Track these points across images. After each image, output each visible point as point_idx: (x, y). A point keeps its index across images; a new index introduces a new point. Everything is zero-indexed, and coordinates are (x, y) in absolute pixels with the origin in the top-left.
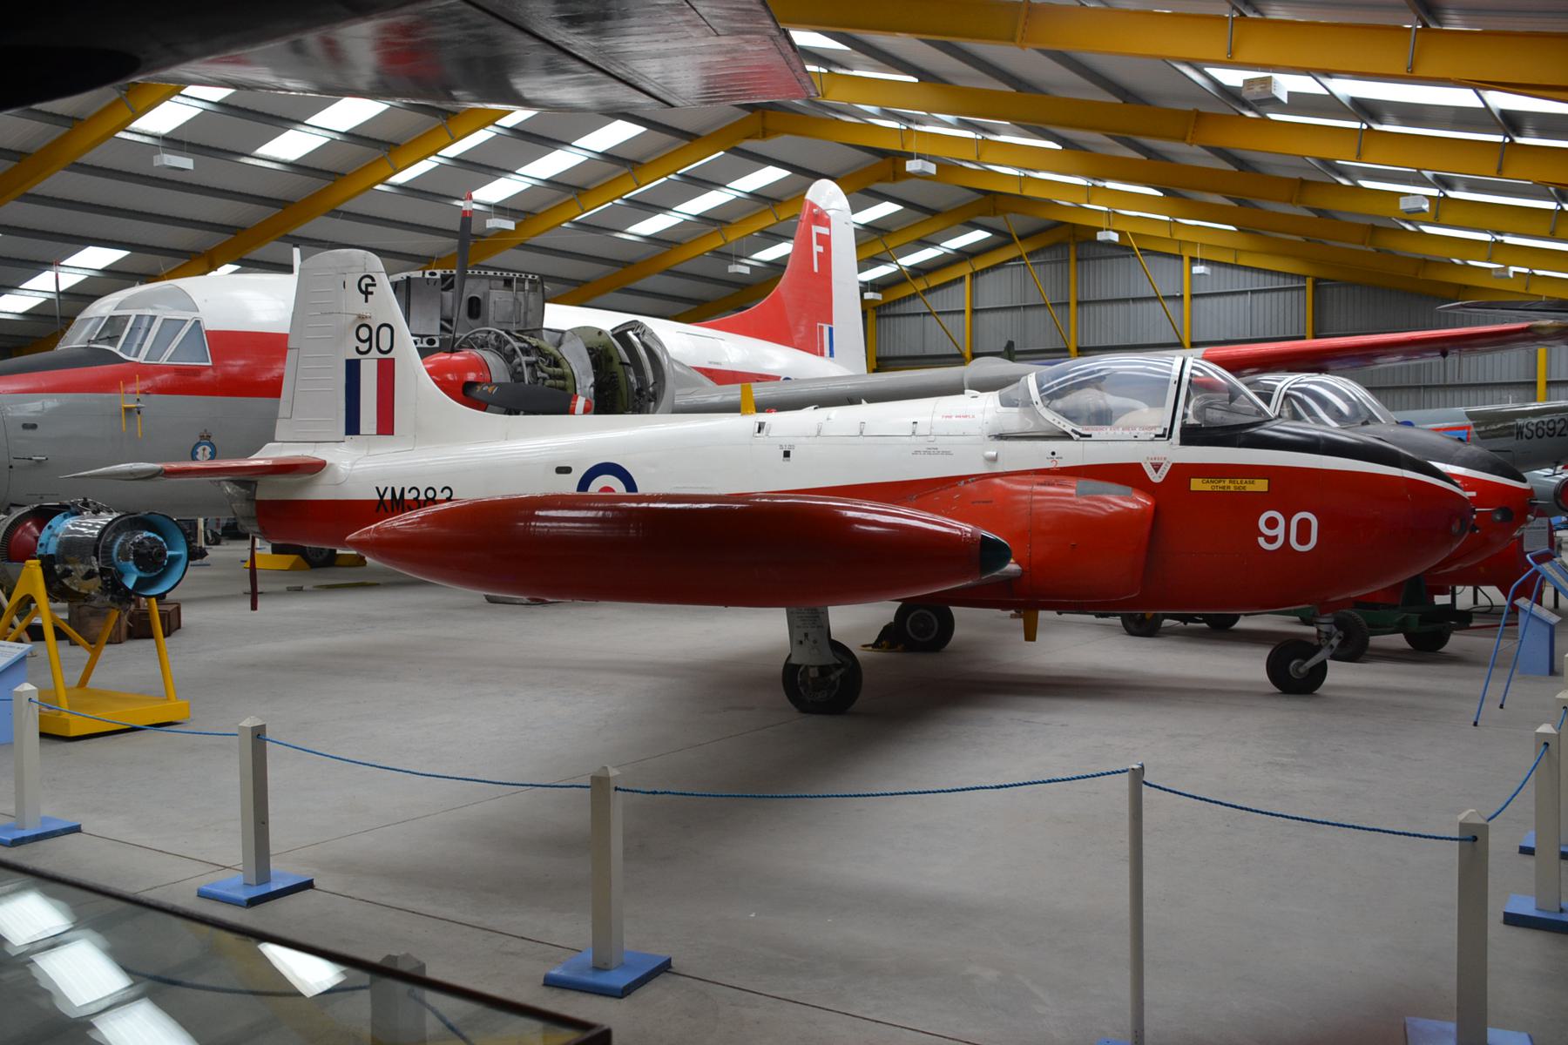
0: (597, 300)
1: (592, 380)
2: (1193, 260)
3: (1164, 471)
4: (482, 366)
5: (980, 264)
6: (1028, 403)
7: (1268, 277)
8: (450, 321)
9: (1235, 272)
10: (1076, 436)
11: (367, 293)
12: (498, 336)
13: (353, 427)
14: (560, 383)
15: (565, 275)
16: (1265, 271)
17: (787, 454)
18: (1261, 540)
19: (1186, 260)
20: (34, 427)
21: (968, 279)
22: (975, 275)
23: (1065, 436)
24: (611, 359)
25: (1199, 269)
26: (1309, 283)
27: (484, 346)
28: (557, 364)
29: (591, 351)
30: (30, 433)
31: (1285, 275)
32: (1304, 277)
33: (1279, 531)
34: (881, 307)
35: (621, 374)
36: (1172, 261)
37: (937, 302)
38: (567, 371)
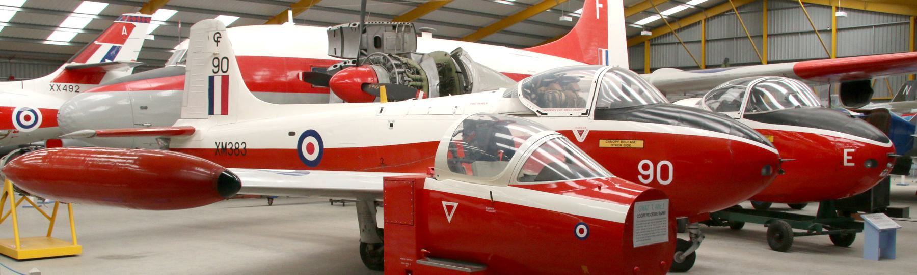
0: (488, 38)
1: (438, 82)
2: (837, 8)
3: (585, 135)
4: (373, 74)
5: (710, 14)
6: (516, 96)
7: (886, 18)
8: (366, 50)
9: (865, 15)
10: (539, 115)
11: (217, 42)
12: (384, 58)
13: (211, 112)
14: (419, 83)
15: (459, 22)
16: (880, 13)
17: (391, 125)
18: (640, 177)
19: (834, 8)
20: (146, 108)
21: (703, 23)
22: (707, 20)
23: (535, 115)
24: (451, 70)
25: (840, 14)
26: (912, 21)
27: (377, 63)
28: (418, 73)
29: (439, 65)
30: (144, 111)
31: (897, 15)
32: (910, 16)
33: (650, 172)
34: (635, 41)
35: (456, 79)
36: (826, 10)
37: (684, 36)
38: (423, 76)
